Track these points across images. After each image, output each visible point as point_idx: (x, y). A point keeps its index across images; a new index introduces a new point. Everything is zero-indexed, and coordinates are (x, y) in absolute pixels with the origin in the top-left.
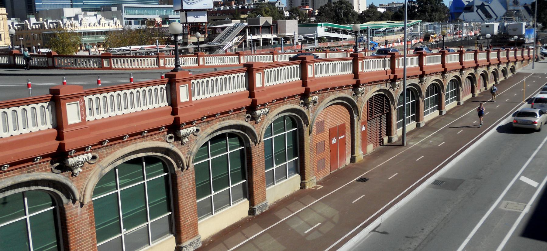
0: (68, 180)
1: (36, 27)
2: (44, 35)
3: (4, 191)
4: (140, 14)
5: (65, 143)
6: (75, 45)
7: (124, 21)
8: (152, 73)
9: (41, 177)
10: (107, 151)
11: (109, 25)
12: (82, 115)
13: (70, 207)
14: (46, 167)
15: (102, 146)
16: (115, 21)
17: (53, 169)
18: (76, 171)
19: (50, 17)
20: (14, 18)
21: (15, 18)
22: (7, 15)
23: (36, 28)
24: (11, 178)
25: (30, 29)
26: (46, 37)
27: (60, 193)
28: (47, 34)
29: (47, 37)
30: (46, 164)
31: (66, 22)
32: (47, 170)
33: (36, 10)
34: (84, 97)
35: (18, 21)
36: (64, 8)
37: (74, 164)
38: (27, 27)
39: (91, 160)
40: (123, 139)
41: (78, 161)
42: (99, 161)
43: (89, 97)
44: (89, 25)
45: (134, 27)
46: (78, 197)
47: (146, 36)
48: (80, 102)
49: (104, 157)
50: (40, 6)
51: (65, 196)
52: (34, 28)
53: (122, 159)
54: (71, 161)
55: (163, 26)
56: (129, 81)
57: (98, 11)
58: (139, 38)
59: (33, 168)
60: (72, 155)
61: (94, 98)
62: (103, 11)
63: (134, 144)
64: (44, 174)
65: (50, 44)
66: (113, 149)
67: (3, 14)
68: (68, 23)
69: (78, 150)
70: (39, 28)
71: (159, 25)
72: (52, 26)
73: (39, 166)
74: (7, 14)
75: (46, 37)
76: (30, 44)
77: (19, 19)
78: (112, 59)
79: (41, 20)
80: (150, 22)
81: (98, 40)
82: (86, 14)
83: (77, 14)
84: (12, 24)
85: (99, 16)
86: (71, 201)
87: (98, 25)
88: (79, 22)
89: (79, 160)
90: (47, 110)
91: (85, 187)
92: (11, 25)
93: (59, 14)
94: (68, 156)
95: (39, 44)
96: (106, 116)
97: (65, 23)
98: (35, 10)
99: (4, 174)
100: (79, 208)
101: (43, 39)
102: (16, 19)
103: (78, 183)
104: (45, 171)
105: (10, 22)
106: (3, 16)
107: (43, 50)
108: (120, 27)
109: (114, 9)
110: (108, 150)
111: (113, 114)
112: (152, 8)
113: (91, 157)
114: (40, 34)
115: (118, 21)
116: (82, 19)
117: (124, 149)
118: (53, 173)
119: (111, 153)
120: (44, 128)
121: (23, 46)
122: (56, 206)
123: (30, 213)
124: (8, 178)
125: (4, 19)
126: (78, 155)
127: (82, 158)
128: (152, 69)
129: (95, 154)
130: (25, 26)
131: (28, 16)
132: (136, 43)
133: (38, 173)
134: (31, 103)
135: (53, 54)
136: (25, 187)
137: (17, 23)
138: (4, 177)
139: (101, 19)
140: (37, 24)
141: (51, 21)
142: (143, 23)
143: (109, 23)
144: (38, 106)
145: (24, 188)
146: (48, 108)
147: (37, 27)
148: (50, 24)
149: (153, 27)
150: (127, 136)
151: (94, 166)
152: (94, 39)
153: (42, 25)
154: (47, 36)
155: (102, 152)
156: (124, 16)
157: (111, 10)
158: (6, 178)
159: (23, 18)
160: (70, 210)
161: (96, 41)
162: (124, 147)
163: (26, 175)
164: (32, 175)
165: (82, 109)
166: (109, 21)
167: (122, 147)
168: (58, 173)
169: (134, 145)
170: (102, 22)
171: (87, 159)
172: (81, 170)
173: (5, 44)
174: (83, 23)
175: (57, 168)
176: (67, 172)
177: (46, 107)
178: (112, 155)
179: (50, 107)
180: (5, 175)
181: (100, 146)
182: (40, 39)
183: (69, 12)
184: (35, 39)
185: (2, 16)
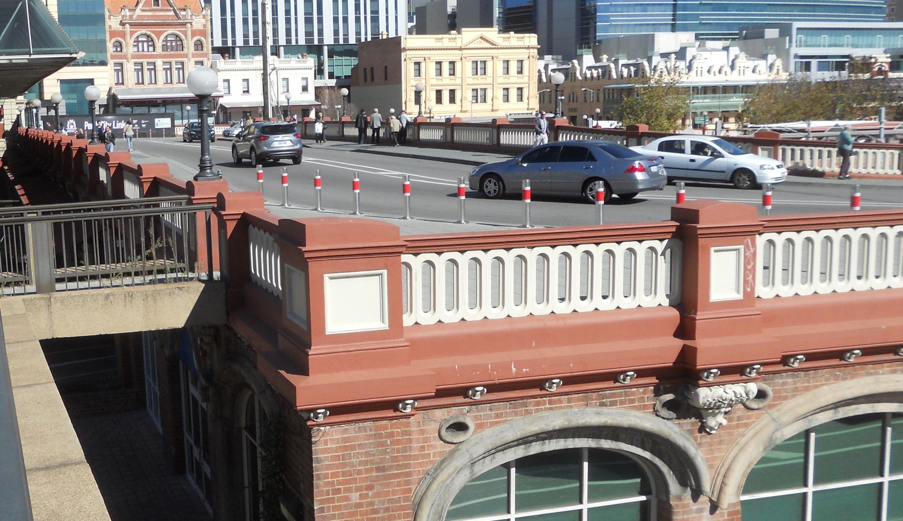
0: (688, 440)
1: (592, 74)
2: (606, 92)
3: (544, 439)
4: (836, 46)
5: (698, 347)
6: (675, 114)
7: (792, 61)
8: (887, 187)
9: (630, 422)
10: (795, 383)
11: (754, 71)
12: (746, 282)
13: (684, 506)
14: (642, 399)
15: (787, 368)
16: (770, 61)
17: (658, 407)
18: (712, 422)
19: (623, 53)
20: (551, 56)
21: (552, 55)
22: (538, 49)
23: (592, 77)
24: (562, 411)
25: (580, 78)
26: (607, 97)
27: (665, 468)
28: (613, 89)
29: (613, 97)
30: (644, 392)
31: (659, 62)
32: (645, 407)
33: (597, 39)
34: (757, 236)
35: (557, 61)
36: (656, 34)
37: (710, 403)
38: (575, 73)
39: (752, 400)
40: (842, 359)
41: (721, 397)
42: (771, 406)
43: (767, 236)
44: (709, 71)
45: (816, 75)
46: (707, 486)
47: (849, 99)
48: (747, 248)
49: (786, 398)
50: (606, 29)
51: (676, 477)
52: (589, 76)
53: (832, 411)
54: (705, 395)
55: (891, 75)
56: (848, 203)
57: (733, 39)
58: (830, 102)
59: (613, 395)
60: (711, 379)
61: (780, 239)
62: (745, 38)
63: (871, 374)
64: (635, 416)
65: (622, 111)
66: (811, 381)
67: (532, 48)
68: (662, 65)
69: (725, 371)
70: (599, 76)
71: (880, 72)
72: (625, 74)
73: (626, 394)
74: (539, 47)
75: (607, 97)
76: (575, 110)
77: (560, 57)
78: (780, 147)
79: (605, 60)
80: (862, 64)
81: (724, 107)
82: (704, 46)
83: (683, 46)
84: (546, 67)
85: (735, 50)
86: (689, 492)
87: (728, 69)
88: (688, 64)
89: (725, 396)
90: (661, 259)
91: (727, 464)
92: (543, 71)
93: (645, 46)
94: (701, 382)
95: (598, 110)
96: (805, 290)
97: (655, 67)
98: (595, 37)
99: (548, 399)
100: (707, 513)
101: (604, 100)
102: (555, 57)
103: (712, 452)
104: (638, 408)
105: (541, 64)
106: (532, 50)
107: (605, 124)
108: (784, 77)
109: (771, 33)
110: (801, 380)
111: (824, 288)
112: (866, 32)
113: (756, 392)
114: (598, 90)
115: (779, 63)
116: (694, 57)
117: (842, 384)
118: (657, 415)
119: (807, 389)
120: (649, 302)
121: (562, 113)
122: (649, 497)
123: (590, 499)
124: (557, 411)
125: (531, 58)
126: (723, 383)
127: (733, 390)
128: (886, 177)
129: (764, 386)
130: (570, 72)
131: (579, 52)
132: (822, 114)
133: (622, 411)
134: (605, 239)
135: (640, 131)
136: (589, 437)
137: (555, 66)
138: (548, 406)
139: (736, 57)
140: (596, 68)
141: (622, 62)
142: (840, 66)
143: (755, 66)
144: (641, 248)
145: (586, 439)
146: (663, 254)
147: (595, 75)
148: (623, 68)
149: (867, 76)
150: (856, 352)
151: (758, 417)
152: (715, 102)
153: (606, 71)
154: (613, 93)
155: (783, 384)
156: (794, 50)
157: (762, 36)
158: (551, 409)
159: (569, 55)
160: (684, 513)
161: (719, 107)
162: (844, 379)
163: (595, 409)
164: (609, 414)
165: (749, 267)
166: (756, 62)
167: (837, 378)
168: (668, 419)
169: (869, 379)
170: (738, 64)
171: (744, 395)
172: (724, 422)
173: (528, 109)
174: (696, 64)
175: (668, 405)
176: (688, 420)
177: (660, 252)
178: (809, 395)
179: (668, 252)
180: (550, 403)
181: (780, 367)
182: (598, 101)
183: (666, 41)
184: (588, 99)
185: (528, 51)
